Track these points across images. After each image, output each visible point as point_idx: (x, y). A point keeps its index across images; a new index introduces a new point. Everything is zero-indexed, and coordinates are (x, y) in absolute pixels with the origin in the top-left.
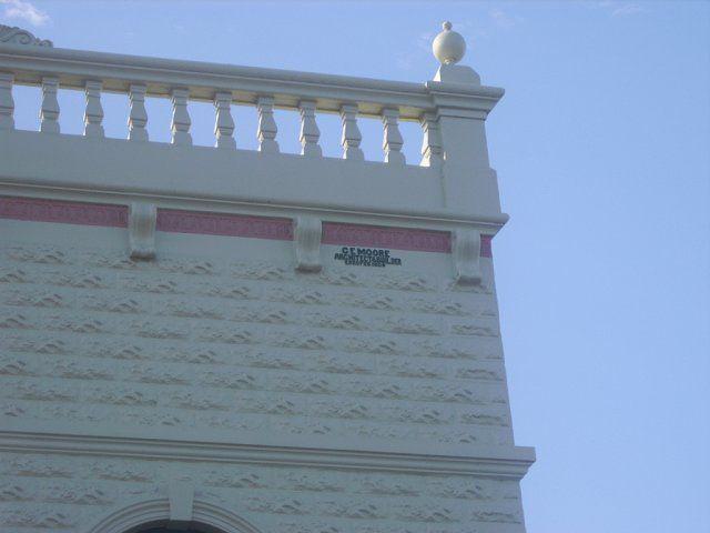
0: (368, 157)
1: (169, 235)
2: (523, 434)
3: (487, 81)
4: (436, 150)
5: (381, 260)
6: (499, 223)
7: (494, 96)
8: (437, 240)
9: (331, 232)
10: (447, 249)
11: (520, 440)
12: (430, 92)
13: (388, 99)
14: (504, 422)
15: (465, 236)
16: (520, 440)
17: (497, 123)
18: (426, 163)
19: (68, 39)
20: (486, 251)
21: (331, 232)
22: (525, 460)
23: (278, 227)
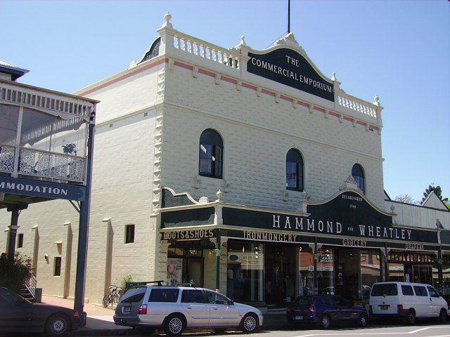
23: (308, 106)
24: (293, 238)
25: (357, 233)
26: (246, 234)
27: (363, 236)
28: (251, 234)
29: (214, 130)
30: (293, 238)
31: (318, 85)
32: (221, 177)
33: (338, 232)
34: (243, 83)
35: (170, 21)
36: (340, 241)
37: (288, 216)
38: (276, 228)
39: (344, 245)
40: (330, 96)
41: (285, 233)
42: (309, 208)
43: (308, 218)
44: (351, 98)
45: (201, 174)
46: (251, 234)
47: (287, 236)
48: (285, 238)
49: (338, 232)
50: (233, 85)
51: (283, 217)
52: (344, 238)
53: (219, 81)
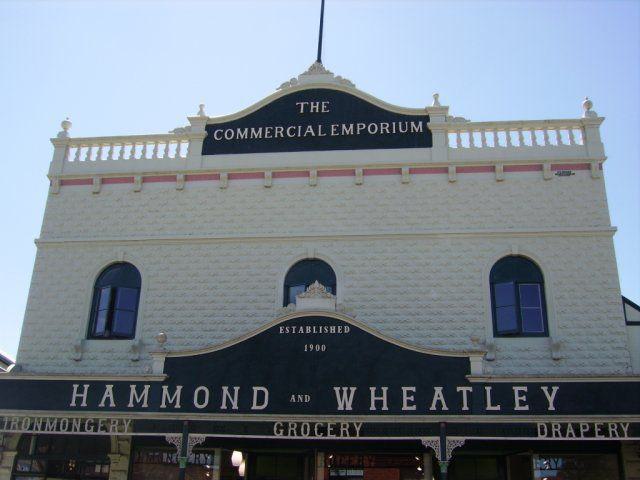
0: (577, 143)
1: (415, 175)
2: (34, 249)
3: (599, 115)
4: (585, 138)
5: (569, 174)
6: (605, 159)
7: (603, 119)
8: (588, 167)
9: (554, 167)
10: (92, 183)
11: (613, 225)
12: (581, 121)
13: (569, 124)
14: (608, 220)
15: (594, 165)
16: (613, 225)
17: (603, 128)
18: (581, 143)
19: (475, 119)
20: (601, 168)
21: (554, 167)
22: (615, 230)
23: (130, 180)
24: (620, 430)
25: (331, 408)
26: (9, 423)
27: (552, 413)
28: (58, 424)
29: (315, 261)
30: (620, 430)
31: (373, 129)
32: (546, 334)
33: (255, 407)
34: (457, 168)
35: (62, 130)
36: (267, 428)
37: (133, 383)
38: (78, 408)
39: (541, 438)
40: (424, 140)
41: (102, 416)
42: (171, 364)
43: (163, 383)
44: (89, 142)
45: (497, 334)
46: (58, 424)
47: (286, 425)
48: (100, 425)
49: (255, 407)
50: (348, 180)
51: (97, 388)
52: (278, 419)
53: (406, 177)
